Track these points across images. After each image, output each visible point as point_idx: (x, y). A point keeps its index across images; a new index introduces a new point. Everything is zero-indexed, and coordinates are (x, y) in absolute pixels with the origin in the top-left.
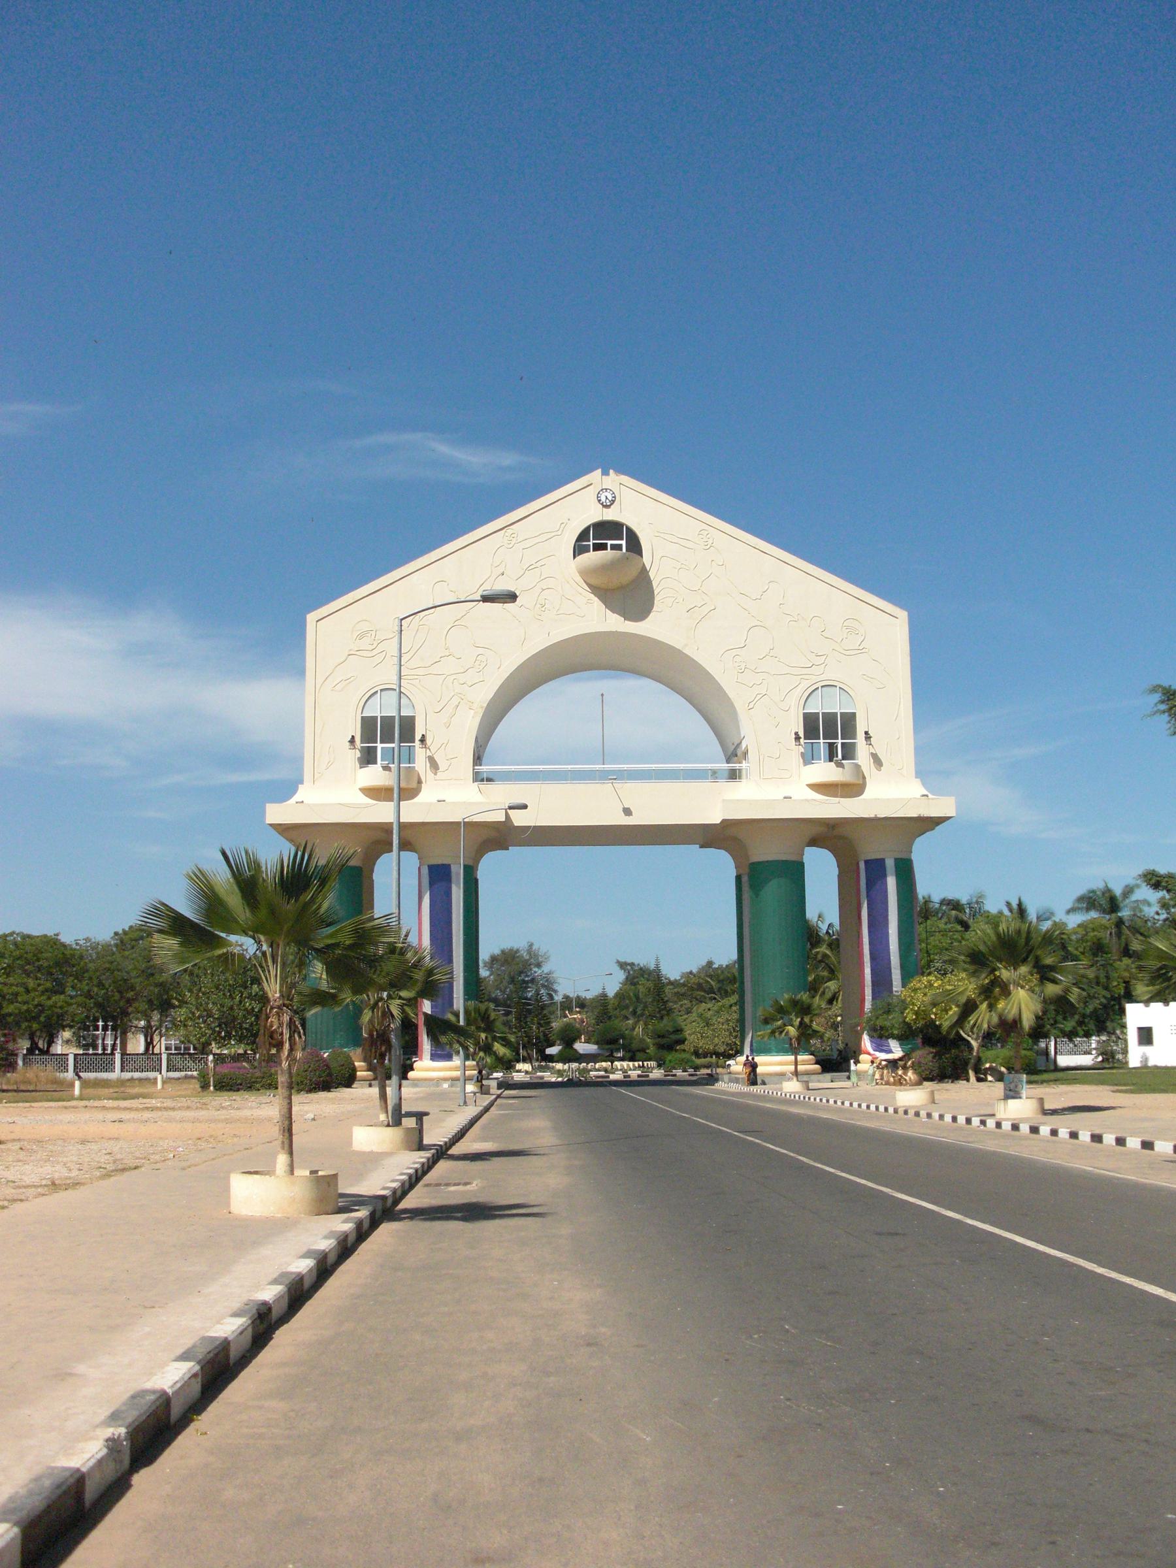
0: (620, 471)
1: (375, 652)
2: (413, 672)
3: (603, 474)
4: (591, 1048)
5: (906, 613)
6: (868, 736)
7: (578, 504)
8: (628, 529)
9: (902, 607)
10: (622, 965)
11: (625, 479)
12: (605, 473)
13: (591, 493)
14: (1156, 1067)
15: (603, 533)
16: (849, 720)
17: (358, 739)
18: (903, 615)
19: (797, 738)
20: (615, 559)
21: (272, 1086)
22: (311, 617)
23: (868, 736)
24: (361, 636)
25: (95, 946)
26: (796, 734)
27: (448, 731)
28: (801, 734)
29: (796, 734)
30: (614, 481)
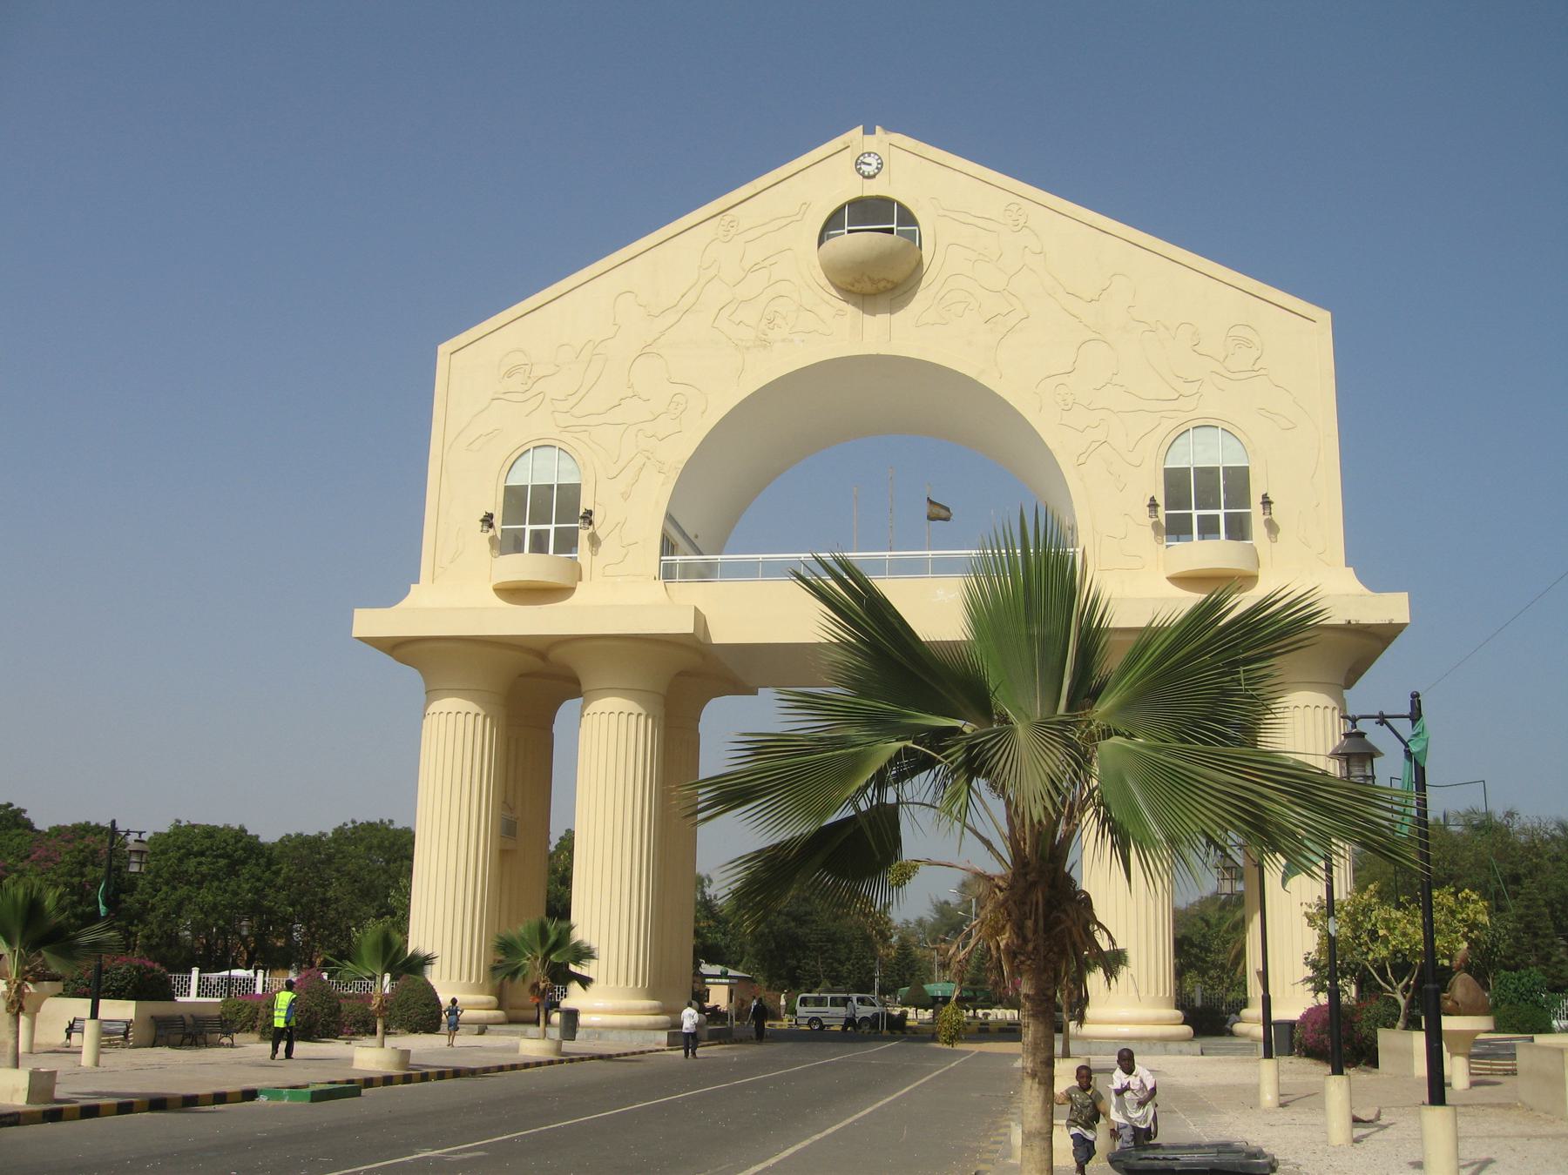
0: (890, 128)
1: (529, 394)
2: (582, 421)
3: (865, 133)
4: (953, 991)
5: (1328, 315)
6: (1266, 502)
7: (828, 175)
8: (900, 206)
9: (1325, 307)
10: (113, 822)
11: (897, 138)
12: (869, 131)
13: (847, 159)
14: (58, 831)
15: (871, 211)
16: (1239, 479)
17: (497, 521)
18: (1324, 317)
19: (1153, 505)
20: (878, 255)
21: (374, 1032)
22: (444, 349)
23: (1266, 502)
24: (509, 374)
25: (1193, 905)
26: (1152, 499)
27: (630, 512)
28: (1161, 500)
29: (1152, 499)
30: (881, 141)
